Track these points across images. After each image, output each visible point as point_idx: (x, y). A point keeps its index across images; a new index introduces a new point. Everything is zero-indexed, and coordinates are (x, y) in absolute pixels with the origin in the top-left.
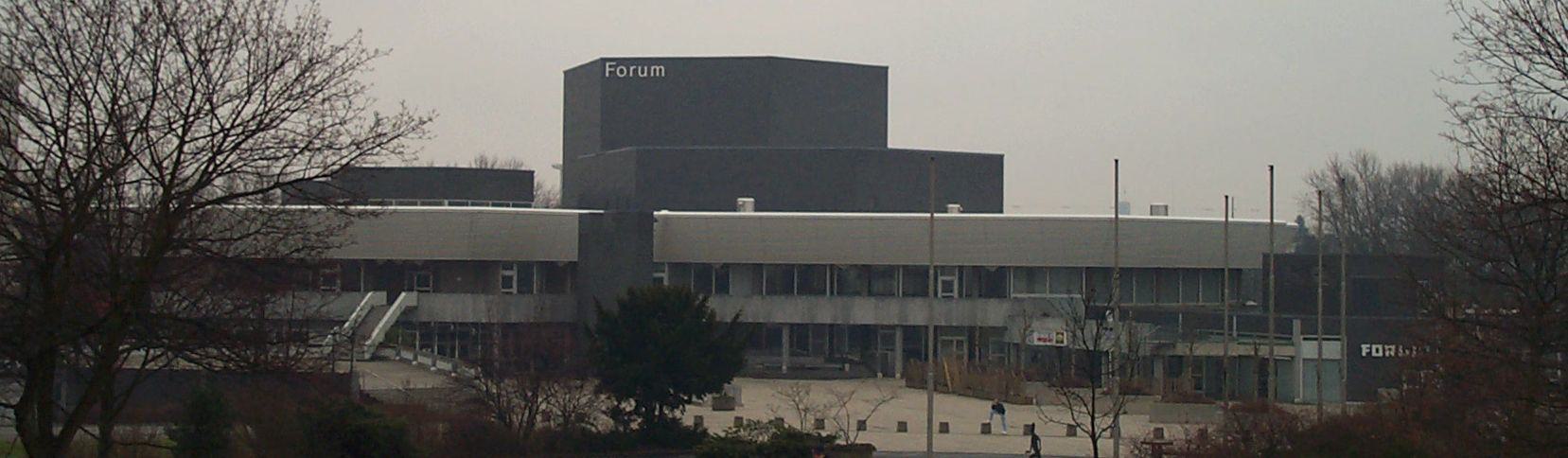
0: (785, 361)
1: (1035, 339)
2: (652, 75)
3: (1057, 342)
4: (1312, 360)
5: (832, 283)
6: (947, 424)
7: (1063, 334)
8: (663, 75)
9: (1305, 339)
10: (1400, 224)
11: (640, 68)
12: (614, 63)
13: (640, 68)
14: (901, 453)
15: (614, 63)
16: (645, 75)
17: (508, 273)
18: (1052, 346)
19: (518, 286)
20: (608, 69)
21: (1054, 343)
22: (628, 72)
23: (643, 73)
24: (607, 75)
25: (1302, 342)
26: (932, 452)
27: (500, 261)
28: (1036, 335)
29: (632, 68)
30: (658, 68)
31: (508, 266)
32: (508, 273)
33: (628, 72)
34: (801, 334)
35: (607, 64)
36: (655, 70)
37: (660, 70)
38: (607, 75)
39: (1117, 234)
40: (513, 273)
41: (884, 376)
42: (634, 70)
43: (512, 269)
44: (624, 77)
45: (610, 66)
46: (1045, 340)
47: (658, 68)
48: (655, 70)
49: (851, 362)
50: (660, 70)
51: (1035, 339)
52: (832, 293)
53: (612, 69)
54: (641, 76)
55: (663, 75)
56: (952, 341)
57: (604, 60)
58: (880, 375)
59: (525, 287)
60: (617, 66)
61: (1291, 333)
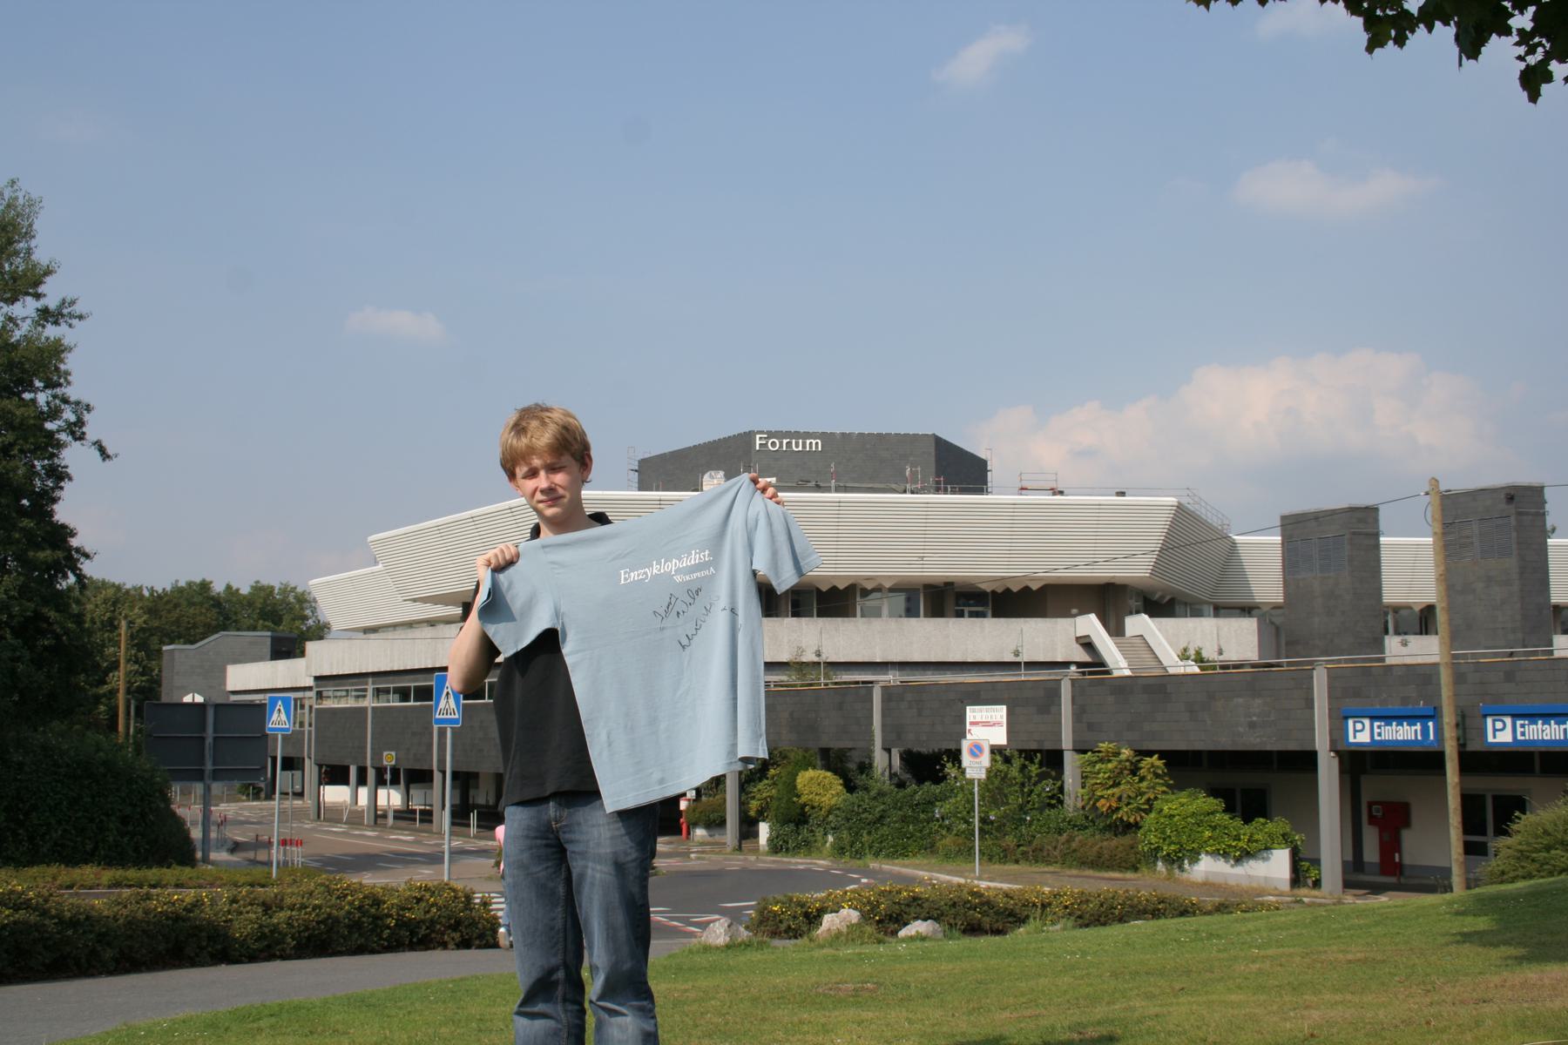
13: (794, 441)
30: (814, 442)
35: (758, 436)
36: (811, 443)
37: (817, 443)
42: (787, 443)
47: (814, 442)
48: (811, 443)
50: (817, 443)
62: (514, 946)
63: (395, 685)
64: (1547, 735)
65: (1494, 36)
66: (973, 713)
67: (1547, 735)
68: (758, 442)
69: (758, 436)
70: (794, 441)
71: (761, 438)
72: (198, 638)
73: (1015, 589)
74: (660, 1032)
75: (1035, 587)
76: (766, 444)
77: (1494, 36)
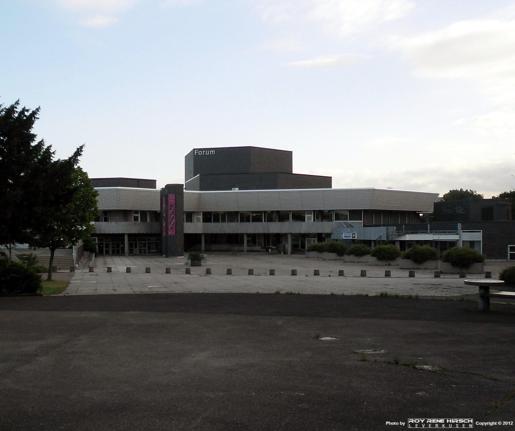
0: (245, 247)
1: (343, 237)
3: (353, 237)
6: (343, 271)
7: (355, 234)
8: (214, 154)
9: (463, 232)
10: (463, 193)
11: (206, 151)
16: (208, 154)
17: (136, 215)
18: (420, 230)
20: (195, 152)
21: (351, 238)
22: (202, 153)
23: (207, 153)
24: (195, 154)
25: (462, 233)
27: (132, 210)
28: (344, 235)
29: (204, 152)
30: (212, 151)
31: (136, 212)
32: (136, 215)
33: (202, 153)
34: (253, 238)
36: (211, 152)
37: (213, 152)
38: (195, 154)
40: (139, 215)
41: (283, 254)
42: (204, 152)
43: (138, 214)
44: (201, 155)
46: (347, 237)
47: (212, 151)
49: (272, 249)
51: (343, 237)
52: (265, 221)
54: (207, 154)
55: (214, 154)
56: (311, 240)
57: (194, 149)
58: (282, 253)
59: (144, 219)
60: (199, 151)
61: (457, 230)
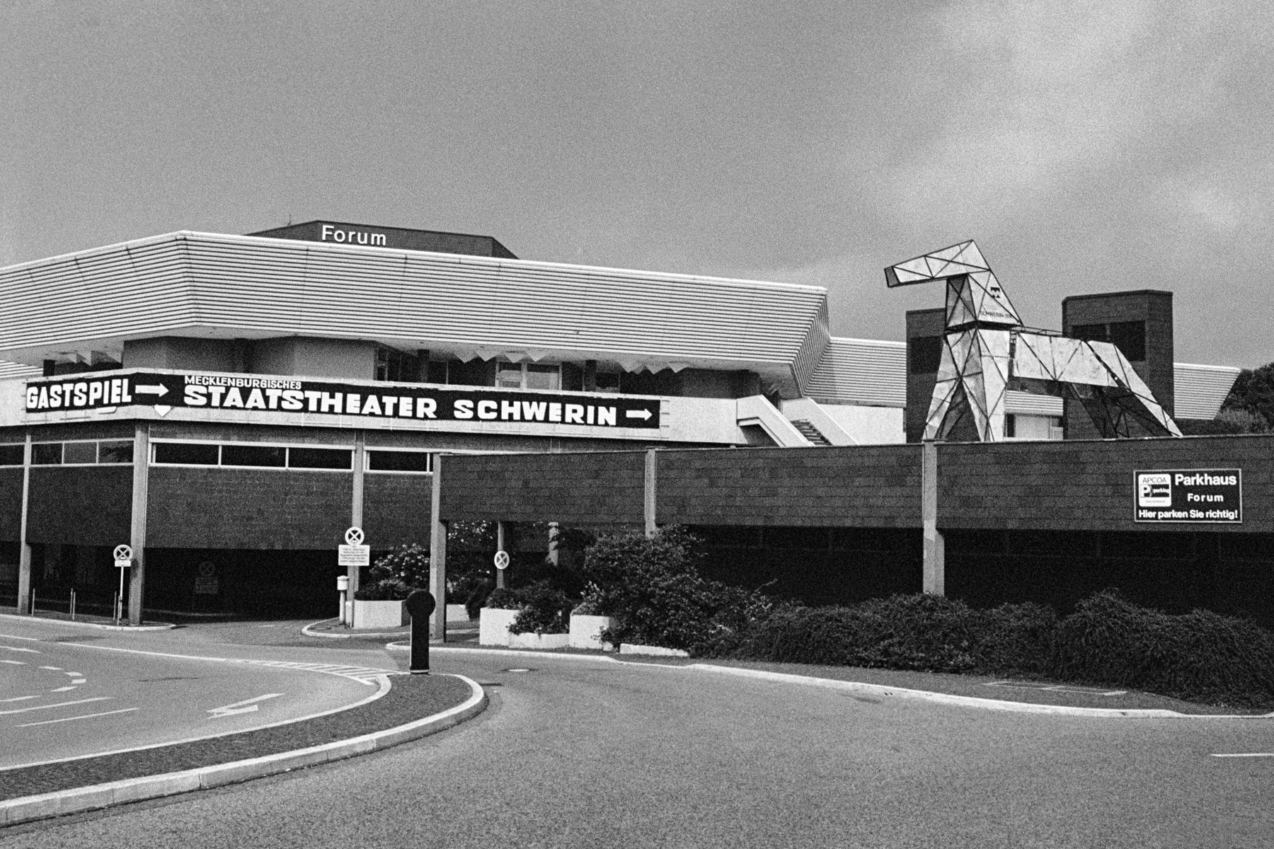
2: (366, 235)
4: (1065, 403)
5: (243, 706)
12: (332, 227)
13: (359, 234)
14: (1034, 680)
15: (332, 227)
19: (101, 467)
26: (1064, 398)
29: (351, 234)
30: (379, 237)
35: (325, 227)
36: (376, 238)
37: (381, 238)
39: (440, 731)
42: (353, 236)
45: (327, 229)
47: (379, 237)
48: (376, 238)
50: (381, 238)
53: (331, 233)
54: (382, 235)
62: (735, 421)
63: (67, 442)
64: (96, 390)
65: (160, 395)
66: (458, 404)
67: (96, 390)
68: (325, 233)
69: (325, 227)
70: (359, 234)
71: (327, 229)
72: (24, 775)
73: (654, 370)
74: (308, 415)
75: (654, 370)
76: (332, 235)
77: (160, 395)
